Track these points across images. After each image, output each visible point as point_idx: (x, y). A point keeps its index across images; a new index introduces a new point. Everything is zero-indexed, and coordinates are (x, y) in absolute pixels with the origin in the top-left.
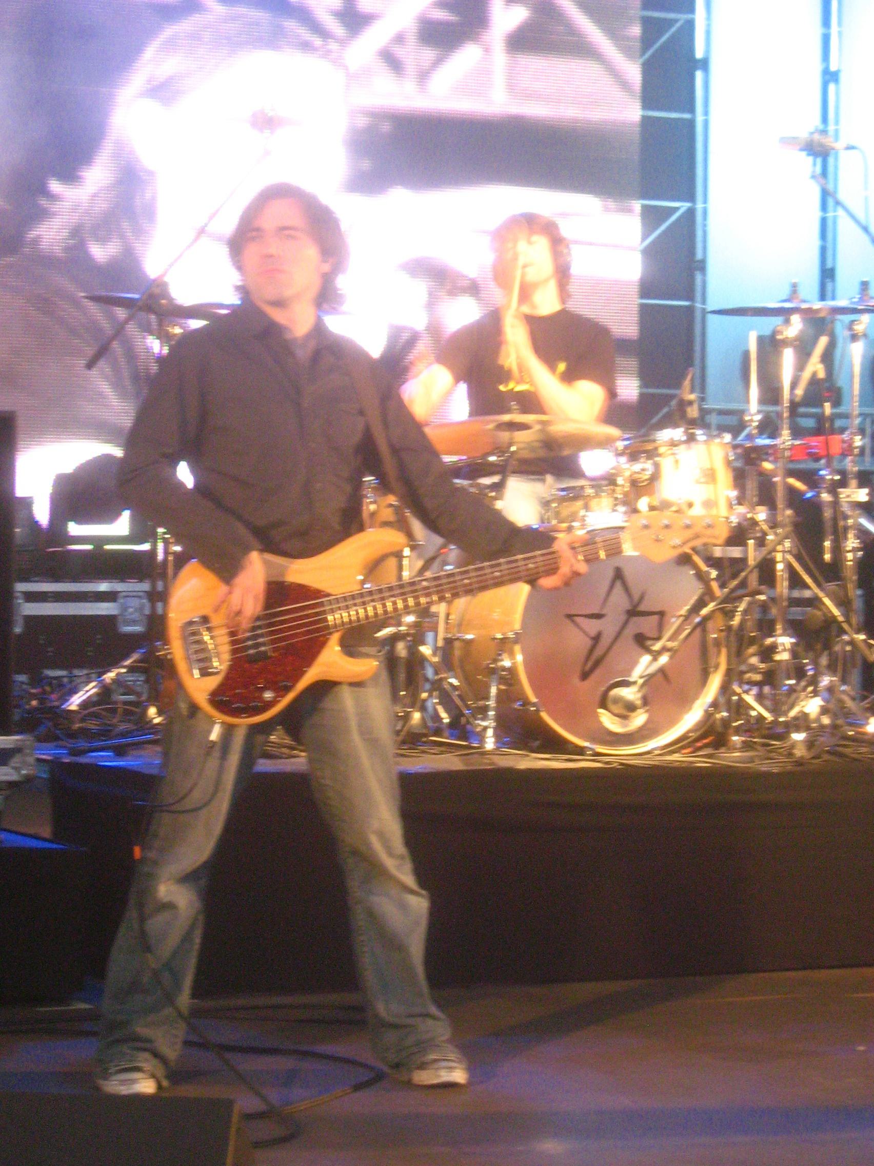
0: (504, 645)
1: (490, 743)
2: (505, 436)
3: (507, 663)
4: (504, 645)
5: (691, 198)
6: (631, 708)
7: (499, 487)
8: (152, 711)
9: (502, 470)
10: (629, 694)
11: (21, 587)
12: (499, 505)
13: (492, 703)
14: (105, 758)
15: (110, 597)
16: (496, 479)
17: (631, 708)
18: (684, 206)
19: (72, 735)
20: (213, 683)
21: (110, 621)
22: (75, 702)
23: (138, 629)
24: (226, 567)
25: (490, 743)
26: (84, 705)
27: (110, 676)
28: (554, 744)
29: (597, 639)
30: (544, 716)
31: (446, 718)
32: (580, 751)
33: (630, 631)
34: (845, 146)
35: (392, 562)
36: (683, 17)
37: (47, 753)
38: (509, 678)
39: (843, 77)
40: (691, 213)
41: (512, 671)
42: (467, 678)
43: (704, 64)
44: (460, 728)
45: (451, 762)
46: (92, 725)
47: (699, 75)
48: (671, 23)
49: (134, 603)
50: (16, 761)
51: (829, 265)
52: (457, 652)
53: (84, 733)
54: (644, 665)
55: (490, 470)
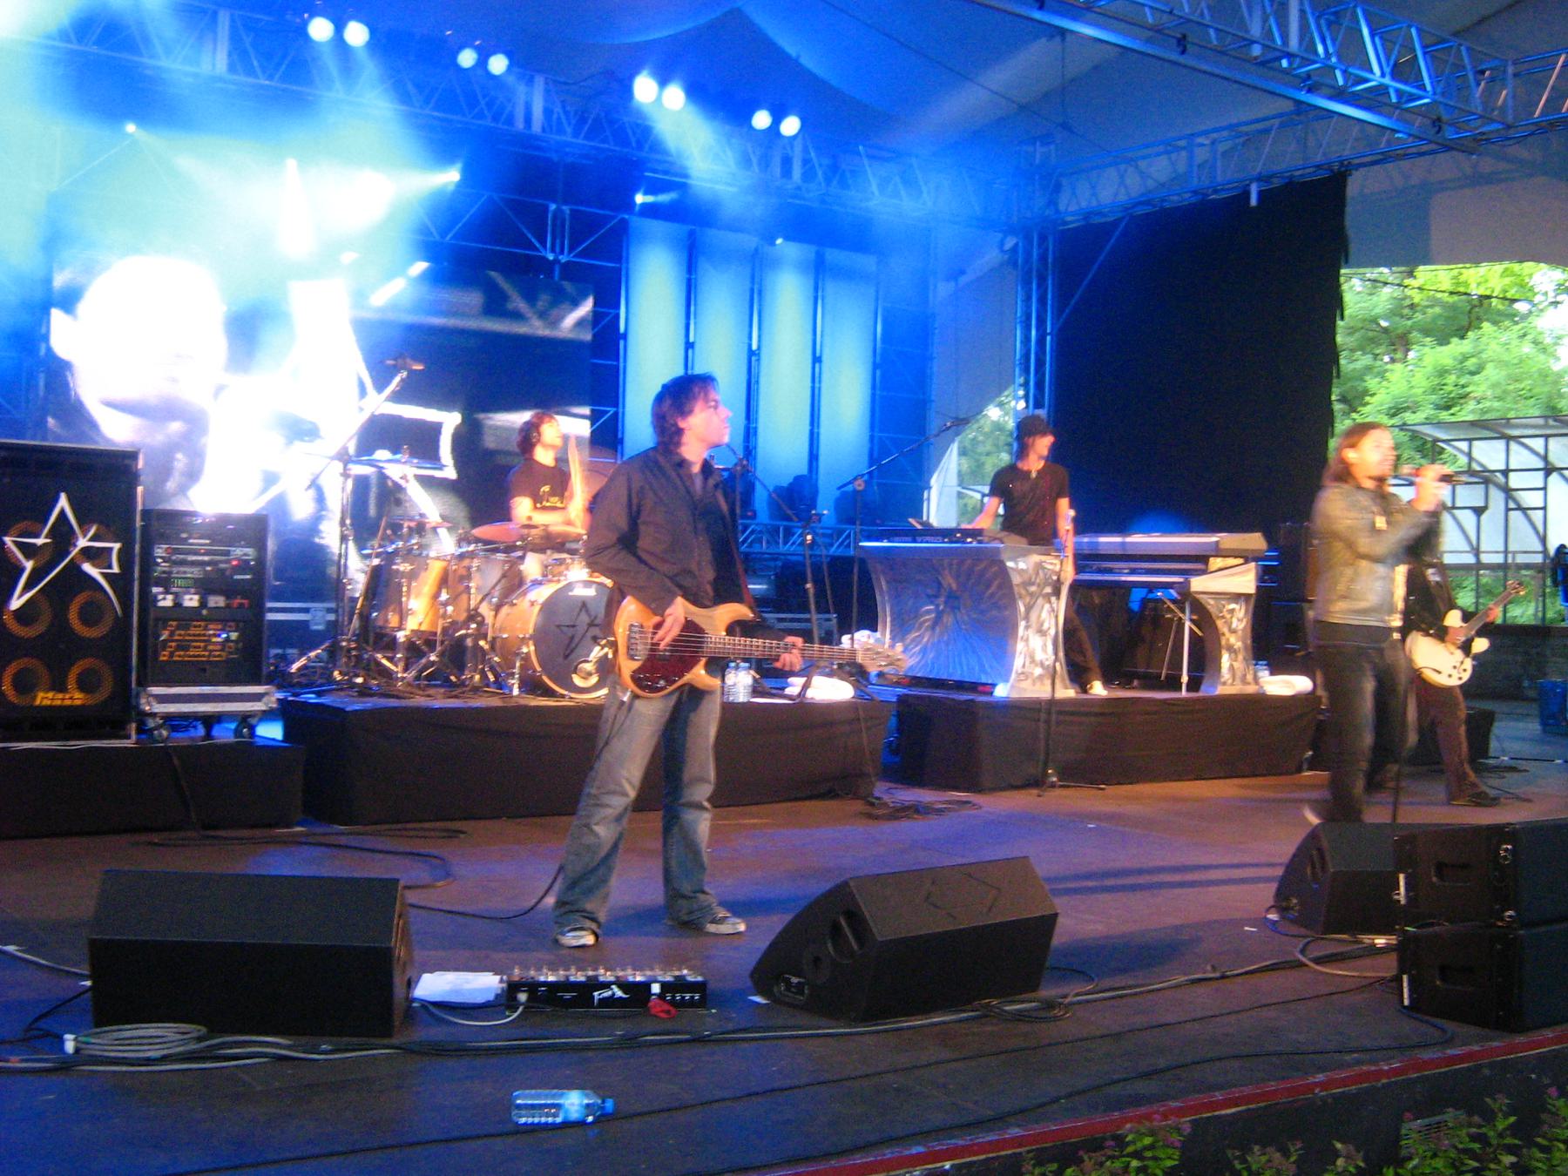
0: (524, 641)
1: (516, 692)
2: (525, 531)
3: (525, 650)
4: (524, 641)
5: (616, 405)
6: (590, 674)
7: (522, 558)
8: (336, 673)
9: (525, 549)
10: (589, 667)
11: (270, 605)
12: (522, 567)
13: (516, 670)
14: (311, 698)
15: (307, 610)
16: (520, 553)
17: (590, 674)
18: (612, 410)
19: (293, 686)
20: (635, 665)
21: (305, 623)
22: (295, 667)
23: (320, 627)
24: (656, 604)
25: (516, 692)
26: (299, 669)
27: (312, 654)
28: (550, 693)
29: (572, 638)
30: (545, 678)
31: (492, 678)
32: (563, 696)
33: (589, 634)
34: (219, 344)
35: (464, 597)
36: (613, 311)
37: (280, 695)
38: (527, 658)
39: (697, 347)
40: (616, 414)
41: (528, 654)
42: (502, 656)
43: (625, 336)
44: (499, 684)
45: (495, 702)
46: (304, 680)
47: (622, 343)
48: (607, 314)
49: (320, 614)
50: (265, 699)
51: (751, 445)
52: (498, 644)
53: (299, 684)
54: (596, 653)
55: (520, 548)
